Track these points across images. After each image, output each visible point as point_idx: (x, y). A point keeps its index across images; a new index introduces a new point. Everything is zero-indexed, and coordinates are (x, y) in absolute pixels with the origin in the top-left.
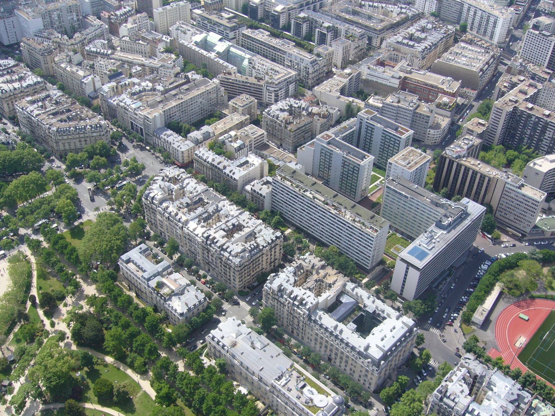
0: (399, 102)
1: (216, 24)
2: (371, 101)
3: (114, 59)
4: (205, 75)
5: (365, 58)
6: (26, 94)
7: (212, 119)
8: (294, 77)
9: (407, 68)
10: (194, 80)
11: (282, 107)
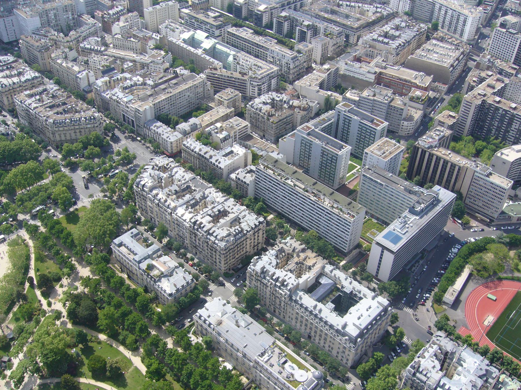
0: (374, 95)
1: (203, 22)
2: (348, 95)
3: (107, 55)
4: (193, 70)
5: (343, 54)
6: (24, 88)
7: (199, 112)
8: (276, 72)
9: (382, 64)
10: (182, 75)
11: (264, 101)
